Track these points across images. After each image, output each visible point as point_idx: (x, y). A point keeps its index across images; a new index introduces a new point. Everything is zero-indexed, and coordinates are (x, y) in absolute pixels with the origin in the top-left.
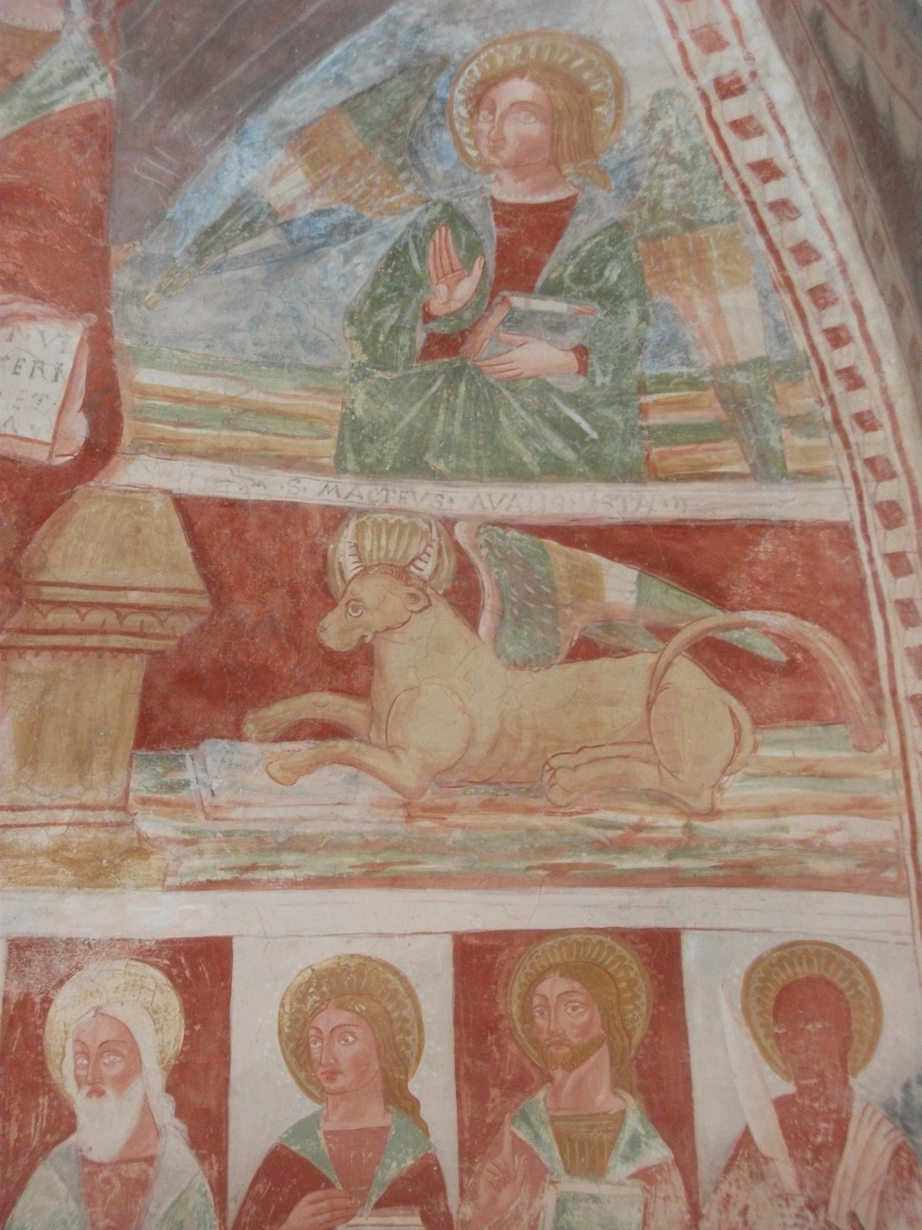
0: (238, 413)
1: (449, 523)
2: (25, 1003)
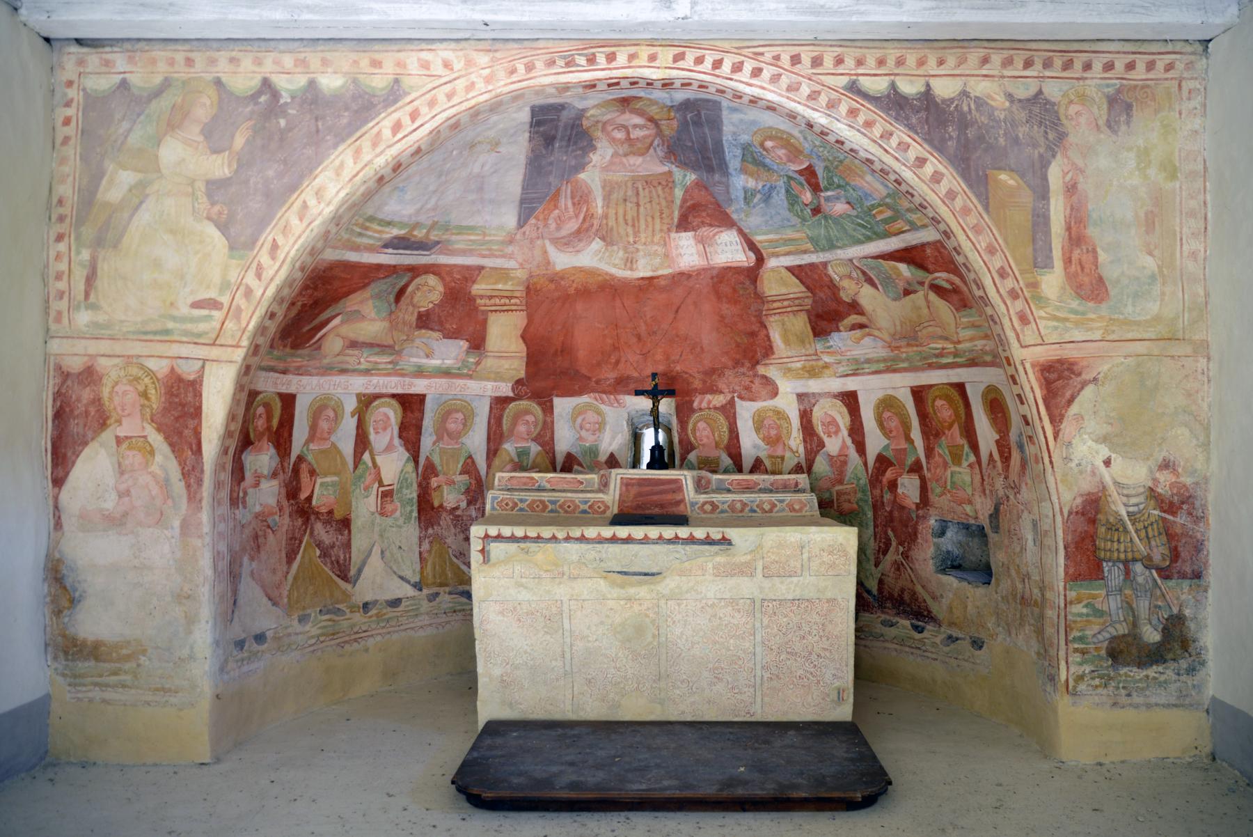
1: (851, 260)
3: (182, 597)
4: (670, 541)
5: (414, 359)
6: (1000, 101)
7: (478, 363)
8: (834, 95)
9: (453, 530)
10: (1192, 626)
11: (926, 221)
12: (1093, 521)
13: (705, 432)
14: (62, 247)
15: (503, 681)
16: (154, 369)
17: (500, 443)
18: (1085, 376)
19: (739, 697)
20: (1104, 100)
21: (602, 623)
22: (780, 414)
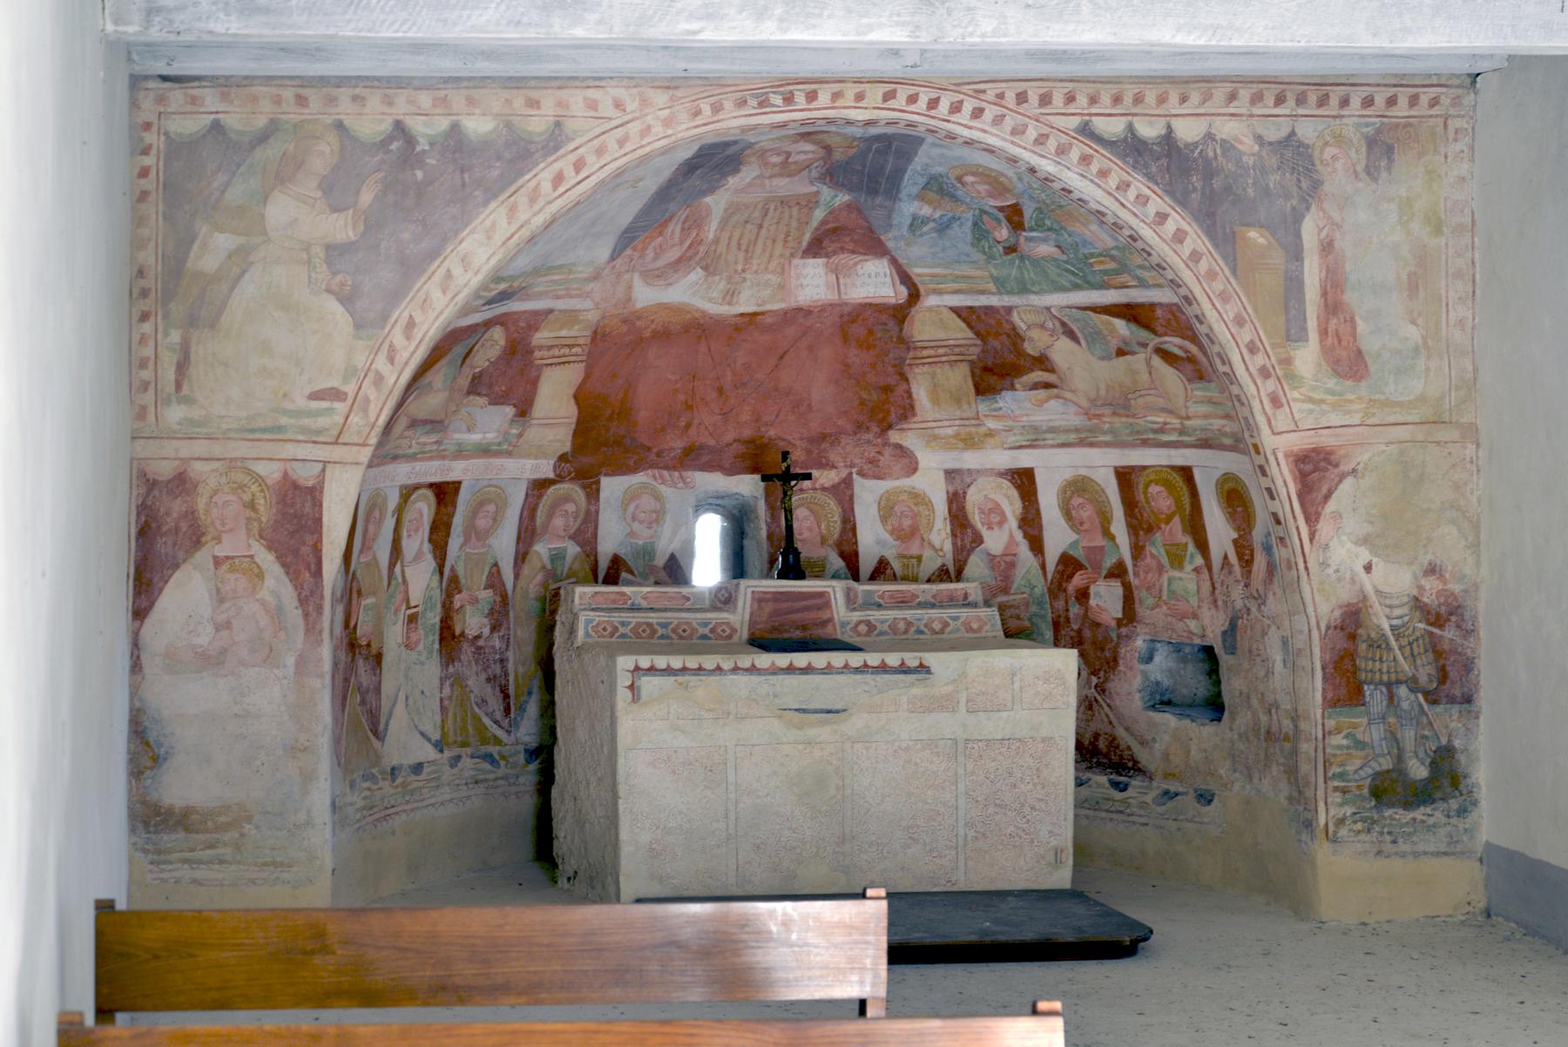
0: (956, 279)
1: (1048, 309)
2: (955, 494)
3: (296, 750)
4: (857, 670)
5: (461, 436)
6: (1248, 145)
7: (520, 435)
8: (1064, 139)
9: (474, 668)
10: (1462, 758)
11: (1161, 281)
12: (1353, 637)
13: (812, 524)
14: (147, 327)
15: (651, 850)
16: (263, 473)
17: (531, 544)
18: (1344, 467)
19: (938, 861)
20: (1363, 142)
21: (775, 773)
22: (918, 497)
